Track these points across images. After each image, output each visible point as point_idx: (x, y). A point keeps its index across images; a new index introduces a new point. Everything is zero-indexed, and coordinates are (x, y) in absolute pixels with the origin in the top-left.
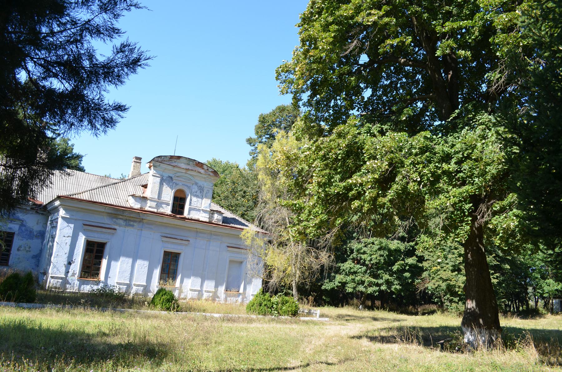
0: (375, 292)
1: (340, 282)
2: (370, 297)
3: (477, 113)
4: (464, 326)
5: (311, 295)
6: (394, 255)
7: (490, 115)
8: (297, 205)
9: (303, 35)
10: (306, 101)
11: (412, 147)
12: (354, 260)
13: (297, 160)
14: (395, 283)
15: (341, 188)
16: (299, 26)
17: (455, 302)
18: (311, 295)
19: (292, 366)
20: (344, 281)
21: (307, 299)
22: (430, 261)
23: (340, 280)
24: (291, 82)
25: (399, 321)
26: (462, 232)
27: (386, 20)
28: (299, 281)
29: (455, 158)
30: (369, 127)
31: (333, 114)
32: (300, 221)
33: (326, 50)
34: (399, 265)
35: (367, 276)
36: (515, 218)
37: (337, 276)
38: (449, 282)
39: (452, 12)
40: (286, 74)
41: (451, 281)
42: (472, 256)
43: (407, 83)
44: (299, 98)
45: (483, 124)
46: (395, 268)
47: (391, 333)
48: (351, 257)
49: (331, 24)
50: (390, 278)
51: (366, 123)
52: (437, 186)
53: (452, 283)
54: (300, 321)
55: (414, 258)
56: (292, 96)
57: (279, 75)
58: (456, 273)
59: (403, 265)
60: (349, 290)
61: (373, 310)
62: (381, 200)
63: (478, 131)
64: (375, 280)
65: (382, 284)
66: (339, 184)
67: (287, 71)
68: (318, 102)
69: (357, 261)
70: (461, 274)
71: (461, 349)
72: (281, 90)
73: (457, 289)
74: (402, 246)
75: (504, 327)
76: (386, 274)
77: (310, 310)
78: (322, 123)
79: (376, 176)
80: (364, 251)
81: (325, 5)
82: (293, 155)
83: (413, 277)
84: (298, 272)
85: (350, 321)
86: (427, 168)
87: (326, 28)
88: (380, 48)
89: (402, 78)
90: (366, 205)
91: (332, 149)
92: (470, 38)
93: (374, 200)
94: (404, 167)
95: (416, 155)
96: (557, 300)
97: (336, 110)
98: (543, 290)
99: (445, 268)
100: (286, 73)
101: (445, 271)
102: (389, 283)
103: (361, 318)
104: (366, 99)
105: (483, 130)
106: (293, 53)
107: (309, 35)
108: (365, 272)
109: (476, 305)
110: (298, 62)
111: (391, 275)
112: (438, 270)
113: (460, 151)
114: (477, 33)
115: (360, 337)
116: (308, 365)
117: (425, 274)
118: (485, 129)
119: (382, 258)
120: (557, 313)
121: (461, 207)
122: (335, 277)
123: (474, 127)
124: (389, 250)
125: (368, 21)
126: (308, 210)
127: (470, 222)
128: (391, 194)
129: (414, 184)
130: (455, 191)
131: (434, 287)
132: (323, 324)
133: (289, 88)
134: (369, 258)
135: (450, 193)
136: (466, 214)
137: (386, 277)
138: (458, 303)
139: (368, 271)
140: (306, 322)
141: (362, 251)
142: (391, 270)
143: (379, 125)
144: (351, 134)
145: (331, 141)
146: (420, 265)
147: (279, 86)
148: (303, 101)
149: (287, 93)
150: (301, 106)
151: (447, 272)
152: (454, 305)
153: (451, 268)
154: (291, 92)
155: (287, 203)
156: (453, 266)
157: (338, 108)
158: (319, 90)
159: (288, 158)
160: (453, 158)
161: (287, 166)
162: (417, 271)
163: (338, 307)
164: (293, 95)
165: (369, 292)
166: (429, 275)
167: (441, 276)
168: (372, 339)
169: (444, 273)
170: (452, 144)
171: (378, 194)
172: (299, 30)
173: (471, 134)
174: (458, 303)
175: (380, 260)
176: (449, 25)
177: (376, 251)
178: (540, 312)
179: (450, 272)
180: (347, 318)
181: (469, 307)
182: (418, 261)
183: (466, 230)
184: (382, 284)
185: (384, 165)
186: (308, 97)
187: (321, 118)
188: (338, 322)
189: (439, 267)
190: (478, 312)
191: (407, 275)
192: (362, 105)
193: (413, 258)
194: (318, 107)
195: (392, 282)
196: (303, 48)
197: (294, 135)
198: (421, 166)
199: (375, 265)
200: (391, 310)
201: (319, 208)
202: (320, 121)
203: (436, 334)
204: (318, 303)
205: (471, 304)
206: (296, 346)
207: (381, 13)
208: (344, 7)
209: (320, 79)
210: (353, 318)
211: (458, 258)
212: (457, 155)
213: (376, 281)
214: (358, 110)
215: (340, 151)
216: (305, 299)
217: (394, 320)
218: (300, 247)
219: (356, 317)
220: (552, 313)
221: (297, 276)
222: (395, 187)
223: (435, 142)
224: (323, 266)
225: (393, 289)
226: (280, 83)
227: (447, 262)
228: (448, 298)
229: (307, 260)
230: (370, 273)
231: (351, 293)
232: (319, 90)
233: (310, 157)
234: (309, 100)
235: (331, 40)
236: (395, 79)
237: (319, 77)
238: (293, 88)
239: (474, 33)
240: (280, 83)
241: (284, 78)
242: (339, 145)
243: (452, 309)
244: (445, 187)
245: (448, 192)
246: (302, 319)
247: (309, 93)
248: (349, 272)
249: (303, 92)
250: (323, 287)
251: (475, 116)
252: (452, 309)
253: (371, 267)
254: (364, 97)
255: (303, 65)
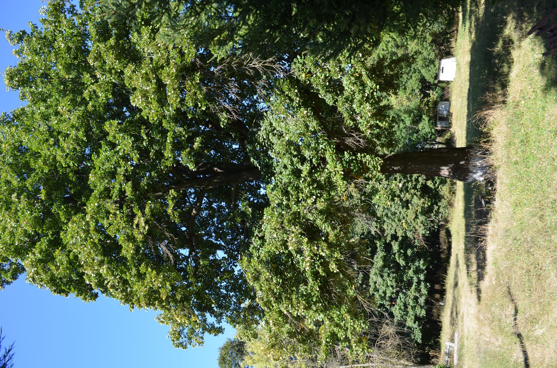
0: (426, 286)
1: (415, 323)
2: (431, 292)
3: (256, 141)
4: (467, 179)
5: (428, 352)
6: (388, 262)
7: (260, 130)
8: (328, 340)
9: (143, 304)
10: (216, 319)
11: (279, 205)
12: (392, 305)
13: (277, 335)
14: (417, 265)
15: (315, 284)
16: (133, 307)
17: (438, 209)
18: (428, 352)
19: (521, 355)
20: (413, 317)
21: (433, 357)
22: (397, 228)
23: (412, 321)
24: (193, 331)
25: (457, 262)
26: (372, 163)
27: (147, 210)
28: (413, 361)
29: (297, 165)
30: (253, 248)
31: (235, 292)
32: (347, 339)
33: (164, 280)
34: (399, 259)
35: (409, 293)
36: (362, 106)
37: (407, 325)
38: (418, 212)
39: (156, 151)
40: (182, 336)
41: (417, 211)
42: (396, 166)
43: (218, 217)
44: (210, 326)
45: (268, 135)
46: (402, 263)
47: (473, 260)
48: (388, 307)
49: (138, 271)
50: (412, 269)
51: (249, 251)
52: (323, 183)
53: (420, 210)
54: (458, 364)
55: (393, 243)
56: (206, 333)
57: (181, 344)
58: (409, 205)
59: (399, 255)
60: (423, 313)
61: (444, 291)
62: (332, 238)
63: (274, 139)
64: (414, 285)
65: (418, 278)
66: (309, 286)
67: (179, 334)
68: (220, 306)
69: (392, 300)
70: (411, 200)
71: (491, 182)
72: (197, 344)
73: (426, 206)
74: (380, 254)
75: (467, 144)
76: (408, 273)
77: (446, 353)
78: (243, 305)
79: (306, 240)
80: (383, 293)
81: (118, 275)
82: (271, 340)
83: (412, 247)
84: (402, 362)
85: (458, 311)
86: (304, 189)
87: (141, 276)
88: (174, 221)
89: (212, 221)
90: (336, 255)
91: (270, 289)
92: (184, 136)
93: (330, 246)
94: (299, 212)
95: (288, 200)
96: (438, 123)
97: (231, 289)
98: (429, 133)
99: (405, 215)
100: (181, 336)
101: (407, 216)
102: (417, 271)
103: (455, 305)
104: (226, 256)
105: (274, 135)
106: (161, 324)
107: (145, 296)
108: (405, 294)
109: (446, 166)
110: (172, 319)
111: (410, 268)
112: (406, 222)
113: (291, 160)
114: (181, 129)
115: (479, 291)
116: (519, 336)
117: (409, 234)
118: (273, 134)
119: (391, 275)
120: (450, 123)
121: (347, 162)
122: (409, 328)
123: (270, 146)
124: (384, 266)
125: (144, 228)
126: (334, 327)
127: (363, 155)
128: (326, 228)
129: (318, 202)
130: (330, 166)
131: (423, 228)
132: (462, 338)
133: (197, 335)
134: (391, 288)
135: (331, 170)
136: (354, 158)
137: (411, 273)
138: (439, 206)
139: (404, 291)
140: (460, 358)
141: (383, 295)
142: (404, 267)
143: (253, 239)
144: (257, 264)
145: (261, 290)
146: (400, 238)
147: (194, 346)
148: (215, 323)
149: (202, 338)
150: (220, 326)
151: (408, 214)
152: (441, 210)
153: (405, 210)
154: (203, 333)
155: (324, 351)
156: (403, 207)
157: (229, 286)
158: (206, 304)
159: (273, 346)
160: (297, 167)
161: (282, 349)
162: (406, 243)
163: (441, 327)
164: (206, 332)
165: (426, 292)
166: (410, 231)
167: (412, 220)
168: (480, 277)
169: (409, 216)
170: (284, 168)
171: (325, 241)
172: (136, 307)
173: (277, 148)
174: (439, 206)
175: (393, 278)
176: (167, 153)
177: (384, 280)
178: (449, 138)
179: (409, 211)
180: (455, 314)
181: (447, 173)
182: (396, 240)
183: (370, 159)
184: (418, 278)
185: (294, 230)
186: (212, 316)
187: (237, 306)
188: (460, 323)
189: (404, 221)
190: (453, 164)
191: (409, 252)
192: (231, 261)
193: (393, 245)
194: (224, 307)
195: (417, 268)
196: (156, 306)
197: (250, 341)
198: (300, 194)
199: (398, 283)
200: (445, 271)
201: (333, 313)
202: (240, 308)
203: (474, 215)
204: (437, 346)
205: (445, 171)
206: (494, 356)
207: (139, 214)
208: (124, 252)
209: (195, 300)
210: (454, 308)
211: (395, 202)
212: (295, 163)
213: (415, 284)
214: (236, 266)
215: (274, 279)
216: (433, 360)
217: (457, 265)
218: (374, 356)
219: (453, 306)
220: (450, 127)
221: (406, 363)
222: (318, 222)
223: (279, 183)
224: (398, 333)
225: (424, 268)
226: (190, 344)
227: (398, 213)
228: (434, 215)
229: (389, 349)
230: (406, 289)
231: (427, 311)
232: (206, 304)
233: (276, 320)
234: (215, 316)
235: (154, 272)
236: (213, 228)
237: (193, 301)
238: (199, 330)
239: (181, 132)
240: (190, 344)
241: (186, 339)
242: (267, 280)
243: (445, 213)
244: (324, 175)
245: (330, 172)
246: (456, 361)
247: (208, 315)
248: (404, 311)
249: (205, 320)
250: (419, 341)
251: (259, 143)
252: (445, 213)
253: (400, 288)
254: (223, 257)
255: (175, 313)
